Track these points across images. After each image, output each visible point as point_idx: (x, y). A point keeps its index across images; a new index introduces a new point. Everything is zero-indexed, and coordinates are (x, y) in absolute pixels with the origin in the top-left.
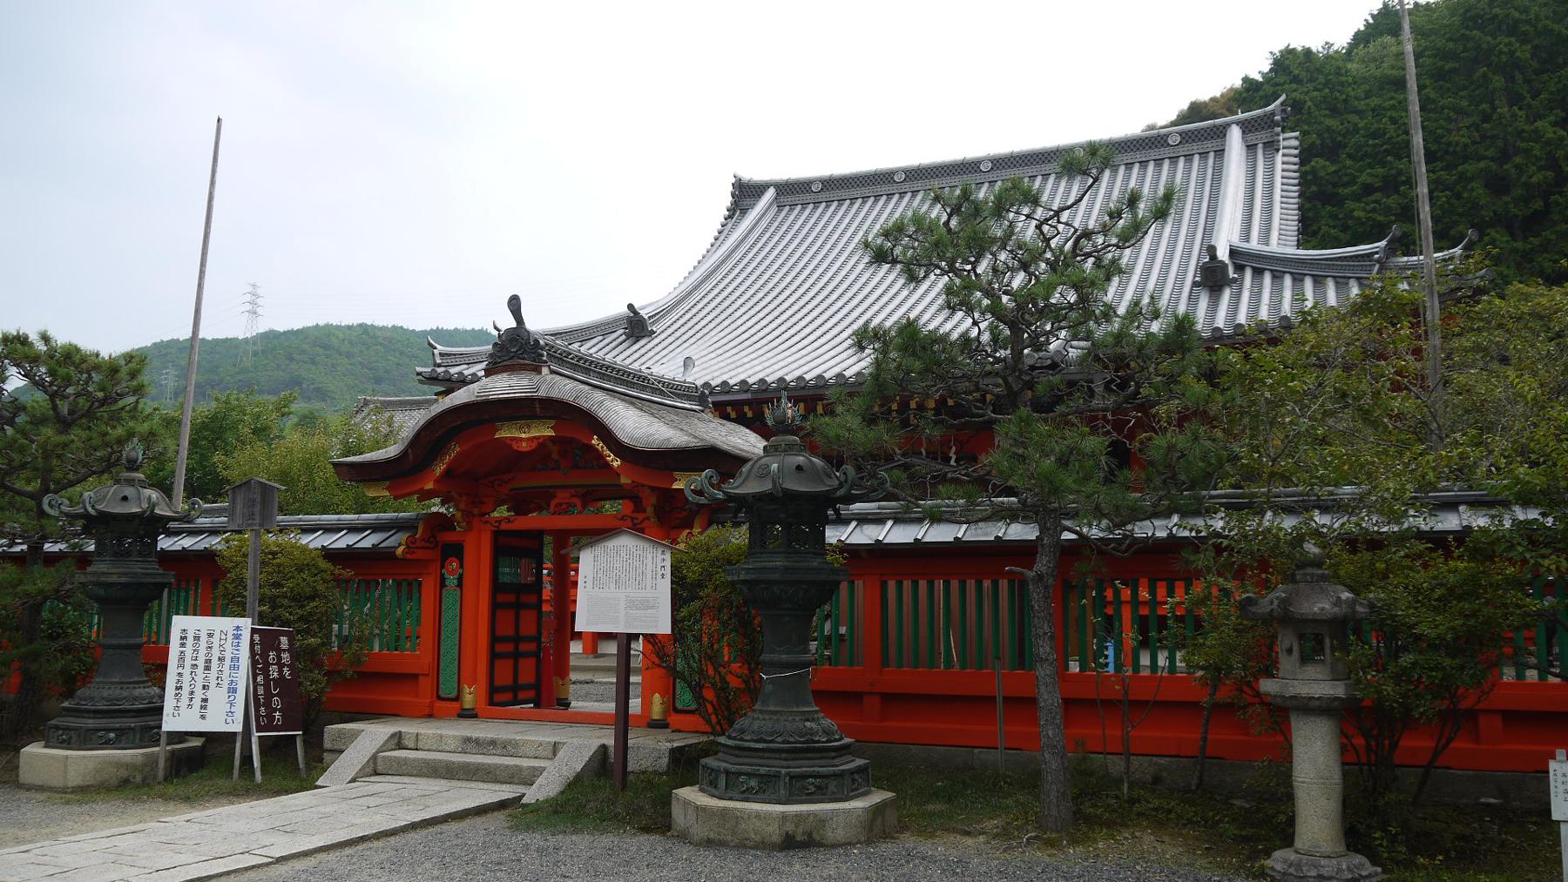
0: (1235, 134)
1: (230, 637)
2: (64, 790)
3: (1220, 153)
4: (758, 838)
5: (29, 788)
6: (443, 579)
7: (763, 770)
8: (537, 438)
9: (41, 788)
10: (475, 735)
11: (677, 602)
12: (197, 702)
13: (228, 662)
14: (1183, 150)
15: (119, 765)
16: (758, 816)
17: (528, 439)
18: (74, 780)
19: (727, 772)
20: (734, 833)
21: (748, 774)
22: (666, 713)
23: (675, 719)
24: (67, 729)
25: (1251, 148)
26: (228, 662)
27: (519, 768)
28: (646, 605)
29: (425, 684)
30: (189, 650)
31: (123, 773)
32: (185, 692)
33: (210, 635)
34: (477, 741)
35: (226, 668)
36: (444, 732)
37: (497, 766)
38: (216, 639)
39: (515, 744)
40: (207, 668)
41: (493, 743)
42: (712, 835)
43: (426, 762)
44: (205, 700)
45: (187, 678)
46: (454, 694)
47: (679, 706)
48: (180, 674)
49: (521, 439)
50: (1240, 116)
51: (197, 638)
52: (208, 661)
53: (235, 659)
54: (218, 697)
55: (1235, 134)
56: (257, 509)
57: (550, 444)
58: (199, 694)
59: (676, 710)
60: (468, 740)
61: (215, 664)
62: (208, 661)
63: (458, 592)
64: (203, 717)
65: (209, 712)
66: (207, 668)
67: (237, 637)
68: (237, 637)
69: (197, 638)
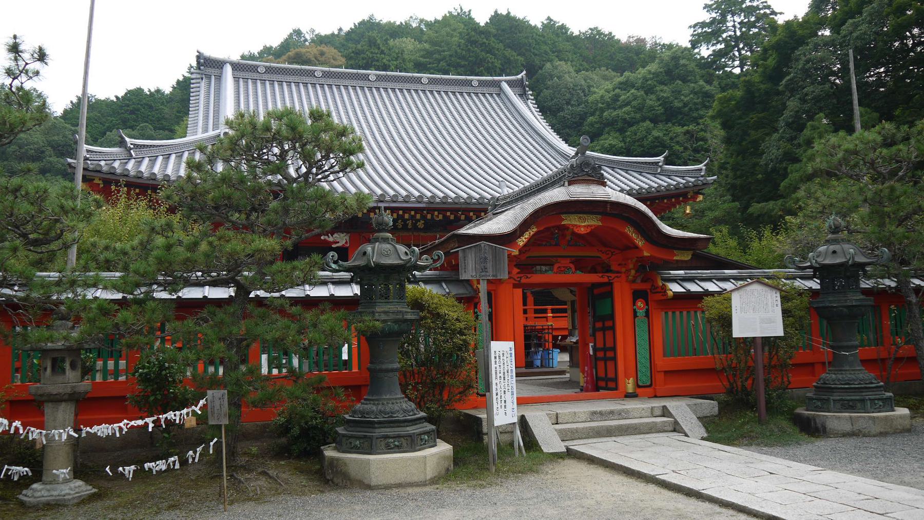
2: (423, 484)
3: (219, 78)
5: (369, 487)
6: (635, 312)
8: (591, 226)
9: (388, 487)
10: (599, 409)
14: (265, 77)
17: (584, 226)
18: (430, 474)
19: (870, 399)
21: (879, 399)
22: (635, 389)
23: (639, 391)
24: (399, 437)
25: (236, 79)
27: (656, 423)
28: (771, 321)
34: (601, 413)
36: (576, 410)
37: (641, 424)
39: (627, 411)
41: (612, 412)
42: (882, 430)
43: (592, 429)
46: (648, 383)
47: (640, 384)
49: (580, 226)
55: (505, 86)
56: (489, 265)
59: (639, 386)
60: (594, 413)
63: (646, 320)
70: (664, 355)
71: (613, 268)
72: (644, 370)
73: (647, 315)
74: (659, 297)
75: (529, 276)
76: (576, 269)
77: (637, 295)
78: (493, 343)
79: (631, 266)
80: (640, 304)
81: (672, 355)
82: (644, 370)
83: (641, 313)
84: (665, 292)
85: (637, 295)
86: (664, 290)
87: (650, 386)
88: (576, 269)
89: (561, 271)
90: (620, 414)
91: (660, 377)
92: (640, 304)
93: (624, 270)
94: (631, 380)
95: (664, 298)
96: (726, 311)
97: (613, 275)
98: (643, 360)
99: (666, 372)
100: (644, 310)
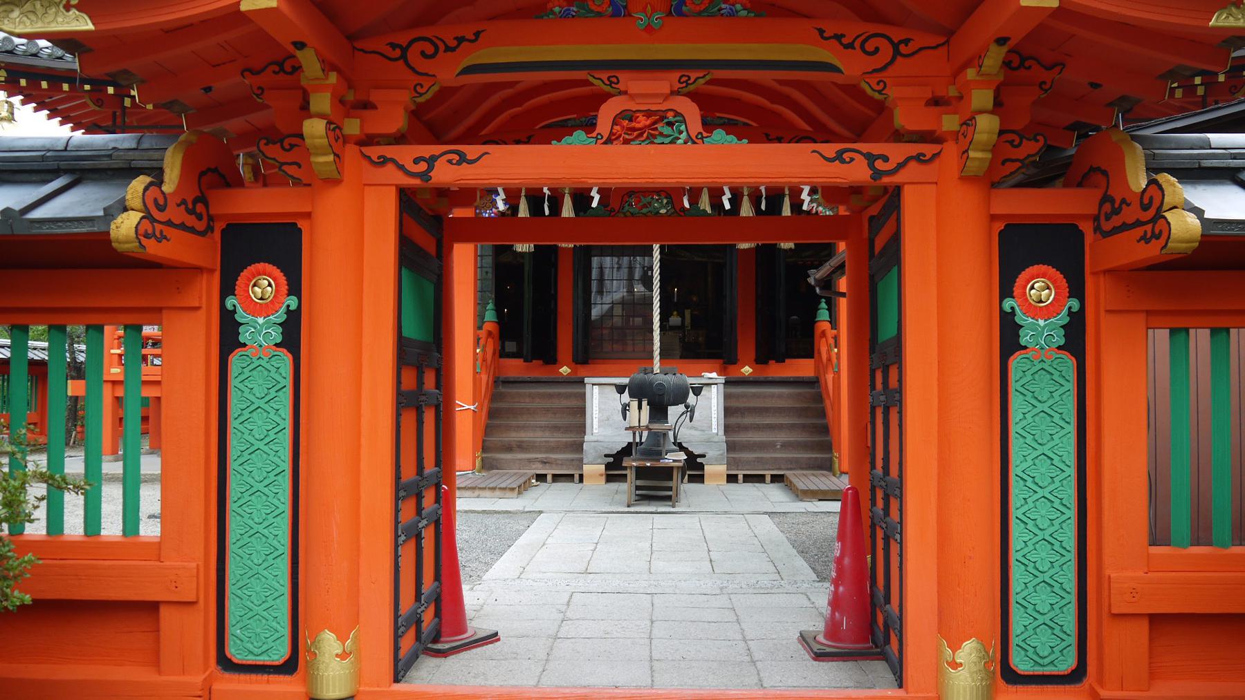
29: (186, 632)
47: (1021, 663)
63: (1068, 364)
70: (1159, 535)
71: (902, 119)
72: (1043, 599)
73: (1075, 338)
74: (1130, 250)
75: (471, 151)
76: (709, 126)
77: (1019, 248)
78: (1208, 331)
79: (982, 98)
80: (1040, 288)
81: (1201, 535)
82: (1043, 599)
83: (1041, 332)
84: (1159, 216)
85: (1019, 248)
86: (1153, 208)
87: (289, 666)
88: (709, 126)
89: (642, 128)
91: (1124, 646)
92: (1040, 288)
93: (950, 123)
94: (968, 652)
95: (1150, 252)
96: (515, 367)
97: (897, 152)
98: (1043, 556)
99: (1155, 620)
100: (1063, 318)
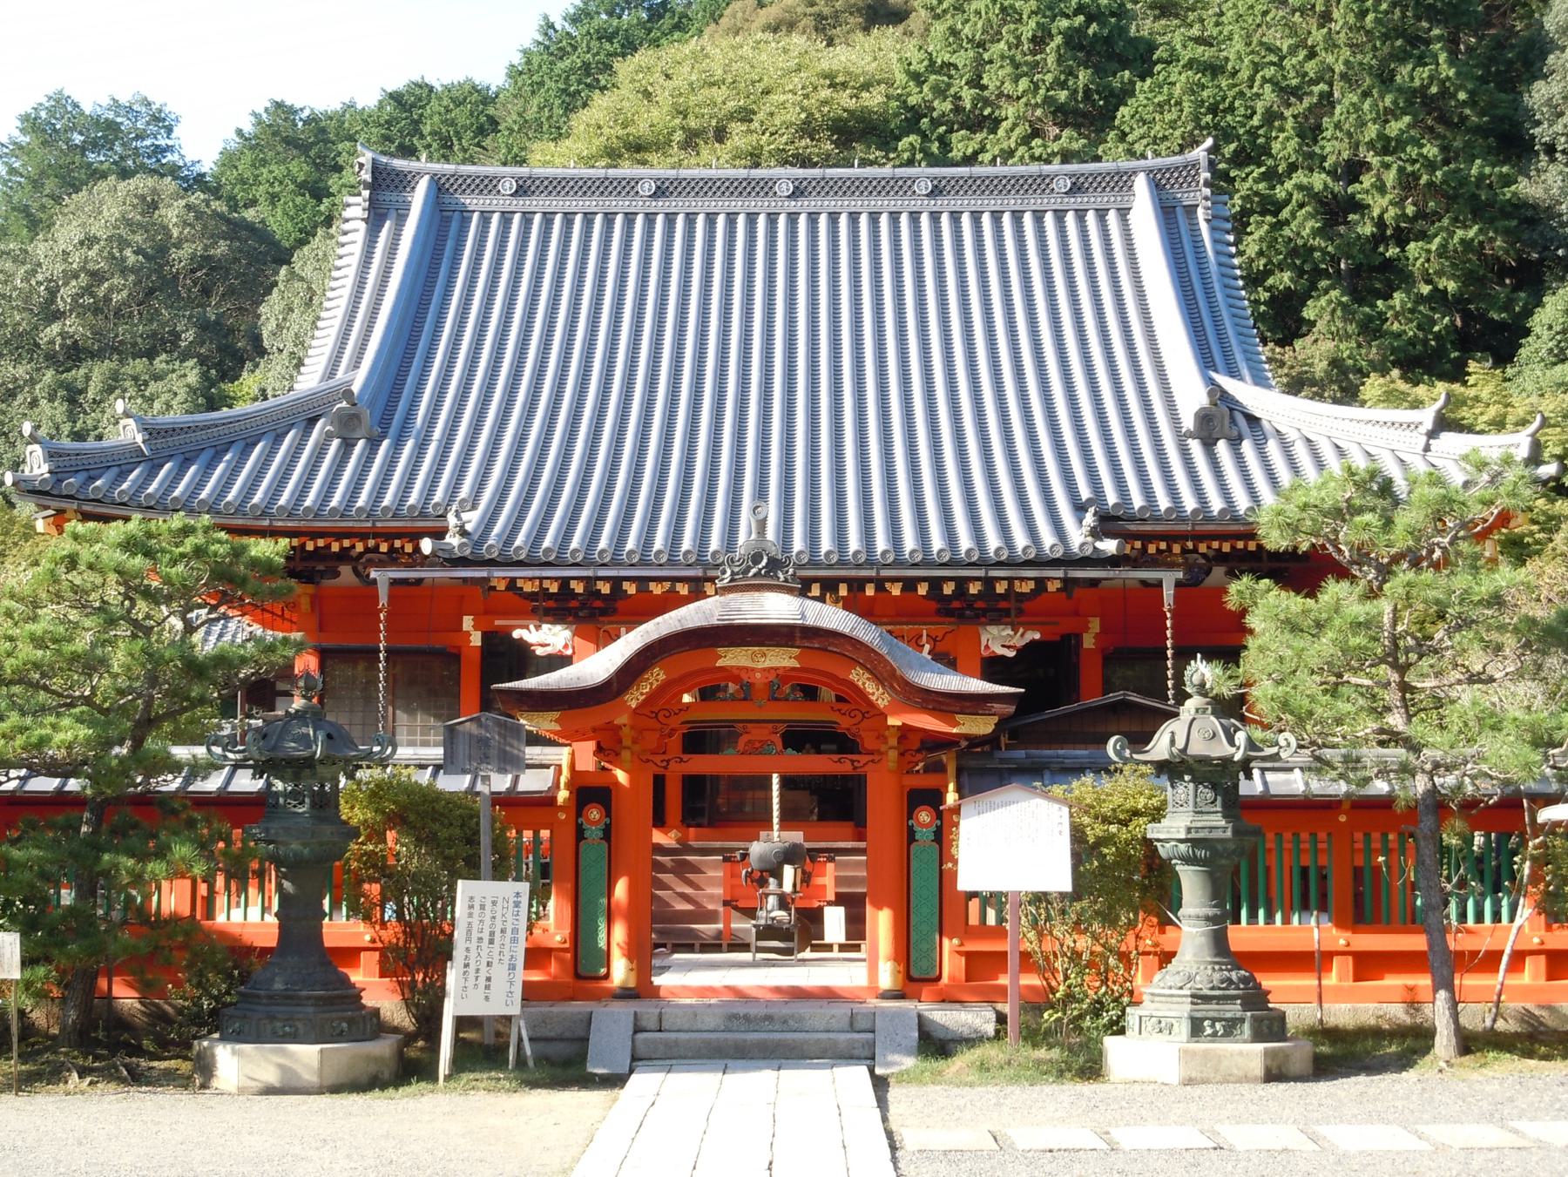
0: (1141, 184)
1: (511, 904)
4: (1241, 1073)
7: (1229, 1015)
11: (1077, 859)
12: (482, 982)
13: (509, 934)
15: (370, 1059)
16: (1241, 1053)
20: (1216, 1071)
26: (509, 934)
27: (835, 1042)
30: (475, 921)
31: (372, 1069)
32: (472, 969)
33: (494, 903)
35: (507, 941)
38: (499, 908)
40: (491, 942)
42: (1193, 1075)
43: (708, 1043)
44: (489, 979)
45: (473, 954)
48: (468, 949)
50: (1152, 161)
51: (482, 907)
52: (492, 934)
53: (515, 931)
54: (499, 973)
55: (1141, 184)
57: (1147, 729)
58: (483, 974)
61: (498, 934)
62: (492, 934)
64: (487, 998)
65: (493, 992)
66: (491, 942)
67: (517, 904)
68: (517, 904)
69: (482, 907)
90: (761, 493)
97: (863, 759)
